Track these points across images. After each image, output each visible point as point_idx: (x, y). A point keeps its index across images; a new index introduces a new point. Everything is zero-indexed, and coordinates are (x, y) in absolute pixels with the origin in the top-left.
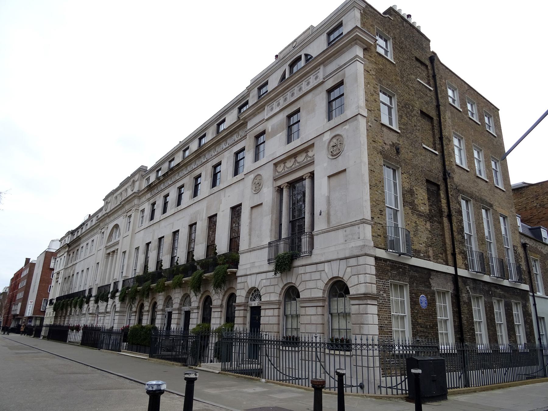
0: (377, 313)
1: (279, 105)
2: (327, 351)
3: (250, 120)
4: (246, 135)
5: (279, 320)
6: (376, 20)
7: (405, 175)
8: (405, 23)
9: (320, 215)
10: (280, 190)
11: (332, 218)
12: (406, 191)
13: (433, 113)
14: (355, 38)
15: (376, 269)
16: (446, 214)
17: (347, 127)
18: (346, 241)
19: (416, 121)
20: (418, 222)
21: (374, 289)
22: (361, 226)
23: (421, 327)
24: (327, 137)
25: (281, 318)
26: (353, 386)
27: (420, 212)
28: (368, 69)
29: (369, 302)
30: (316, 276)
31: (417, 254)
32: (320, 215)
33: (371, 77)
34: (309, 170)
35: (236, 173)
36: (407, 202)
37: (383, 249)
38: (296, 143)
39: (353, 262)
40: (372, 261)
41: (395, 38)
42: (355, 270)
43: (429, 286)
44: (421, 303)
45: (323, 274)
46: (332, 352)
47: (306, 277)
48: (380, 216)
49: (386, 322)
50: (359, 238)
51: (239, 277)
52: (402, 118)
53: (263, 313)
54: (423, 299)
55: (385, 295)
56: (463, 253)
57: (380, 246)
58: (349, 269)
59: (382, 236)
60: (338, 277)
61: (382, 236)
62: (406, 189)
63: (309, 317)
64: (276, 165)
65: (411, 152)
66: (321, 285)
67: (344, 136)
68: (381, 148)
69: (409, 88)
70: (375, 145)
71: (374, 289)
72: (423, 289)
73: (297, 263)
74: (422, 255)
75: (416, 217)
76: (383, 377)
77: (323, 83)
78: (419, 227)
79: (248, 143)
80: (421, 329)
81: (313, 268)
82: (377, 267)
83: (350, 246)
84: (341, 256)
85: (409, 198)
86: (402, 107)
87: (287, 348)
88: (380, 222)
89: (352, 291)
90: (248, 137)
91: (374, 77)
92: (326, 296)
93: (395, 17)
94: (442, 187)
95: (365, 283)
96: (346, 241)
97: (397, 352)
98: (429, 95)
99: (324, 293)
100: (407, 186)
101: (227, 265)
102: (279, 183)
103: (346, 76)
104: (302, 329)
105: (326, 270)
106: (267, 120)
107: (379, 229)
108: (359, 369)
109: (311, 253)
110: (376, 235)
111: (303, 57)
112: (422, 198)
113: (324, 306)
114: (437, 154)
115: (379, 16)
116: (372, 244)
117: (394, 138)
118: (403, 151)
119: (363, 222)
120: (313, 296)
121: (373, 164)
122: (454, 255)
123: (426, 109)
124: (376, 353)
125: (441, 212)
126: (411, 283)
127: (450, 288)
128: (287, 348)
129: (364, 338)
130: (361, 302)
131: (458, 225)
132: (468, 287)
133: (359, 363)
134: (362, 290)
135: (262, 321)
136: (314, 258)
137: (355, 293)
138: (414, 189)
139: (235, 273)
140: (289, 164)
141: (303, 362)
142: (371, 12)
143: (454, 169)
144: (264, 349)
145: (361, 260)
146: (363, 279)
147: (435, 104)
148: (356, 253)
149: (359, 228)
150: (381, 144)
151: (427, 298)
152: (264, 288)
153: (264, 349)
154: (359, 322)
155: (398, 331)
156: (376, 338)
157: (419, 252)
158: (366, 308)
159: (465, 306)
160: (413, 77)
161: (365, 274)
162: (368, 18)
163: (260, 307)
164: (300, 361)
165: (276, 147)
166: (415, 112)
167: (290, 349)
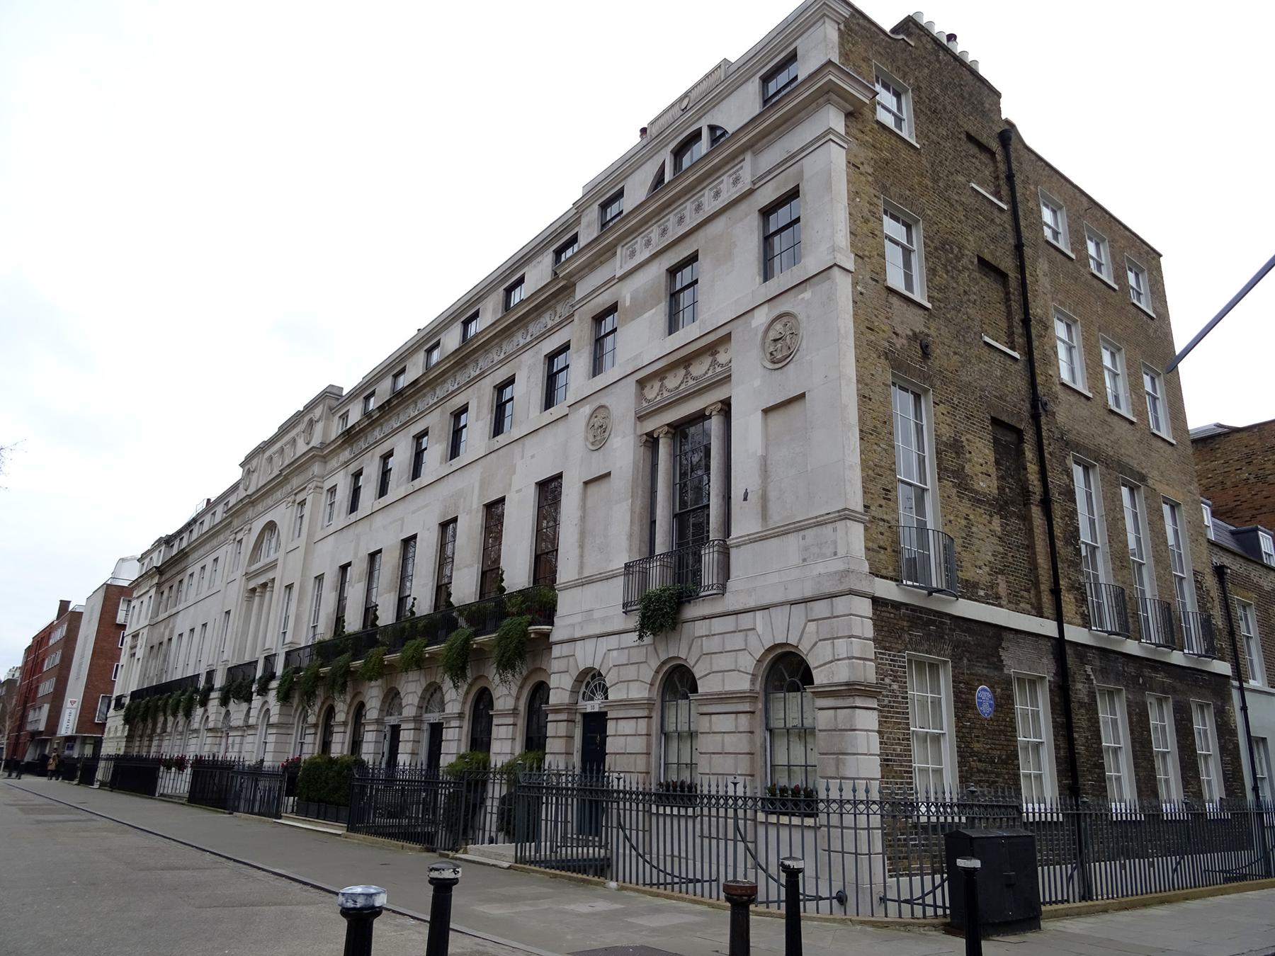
0: (876, 728)
1: (648, 243)
2: (761, 816)
3: (581, 278)
4: (572, 315)
5: (649, 745)
6: (875, 48)
7: (942, 408)
8: (941, 54)
9: (745, 499)
10: (651, 442)
11: (773, 508)
12: (946, 444)
13: (1007, 264)
14: (826, 89)
15: (875, 625)
16: (1038, 497)
17: (807, 295)
18: (804, 560)
19: (967, 280)
20: (971, 517)
21: (869, 673)
22: (840, 525)
23: (980, 761)
24: (761, 318)
25: (654, 739)
26: (821, 899)
27: (977, 492)
28: (857, 162)
29: (859, 702)
30: (736, 641)
31: (969, 590)
32: (745, 499)
33: (863, 178)
34: (718, 395)
35: (549, 402)
36: (946, 469)
37: (891, 579)
38: (688, 333)
39: (820, 608)
40: (865, 607)
41: (919, 88)
42: (825, 629)
43: (999, 666)
44: (980, 704)
45: (752, 638)
46: (773, 819)
47: (713, 644)
48: (883, 502)
49: (898, 748)
50: (835, 554)
51: (556, 643)
52: (934, 275)
53: (611, 727)
54: (983, 695)
55: (895, 686)
56: (1078, 589)
57: (884, 572)
58: (812, 627)
59: (889, 550)
60: (787, 644)
61: (889, 550)
62: (944, 439)
63: (718, 737)
64: (641, 383)
65: (955, 353)
66: (748, 663)
67: (799, 317)
68: (887, 344)
69: (952, 205)
70: (873, 338)
71: (869, 673)
72: (985, 671)
73: (692, 611)
74: (982, 593)
75: (968, 504)
76: (891, 876)
77: (751, 192)
78: (974, 529)
79: (578, 333)
80: (980, 765)
81: (729, 623)
82: (878, 621)
83: (815, 573)
84: (793, 596)
85: (951, 461)
86: (936, 249)
87: (668, 811)
88: (885, 517)
89: (819, 678)
90: (576, 318)
91: (870, 179)
92: (758, 687)
93: (919, 39)
94: (1029, 436)
95: (849, 658)
96: (804, 560)
97: (923, 819)
98: (997, 220)
99: (753, 682)
100: (947, 433)
101: (528, 617)
102: (650, 425)
103: (806, 176)
104: (703, 765)
105: (759, 629)
106: (622, 278)
107: (882, 534)
108: (836, 858)
109: (723, 589)
110: (875, 547)
111: (705, 134)
112: (981, 461)
113: (753, 713)
114: (1016, 359)
115: (882, 36)
116: (866, 567)
117: (916, 322)
118: (937, 351)
119: (845, 515)
120: (728, 688)
121: (869, 381)
122: (1056, 592)
123: (992, 253)
124: (876, 821)
125: (1025, 493)
126: (956, 659)
127: (1046, 669)
128: (668, 811)
129: (848, 785)
130: (840, 703)
131: (1067, 524)
132: (1088, 668)
133: (836, 845)
134: (842, 674)
135: (610, 747)
136: (732, 601)
137: (825, 682)
138: (963, 439)
139: (547, 635)
140: (672, 381)
141: (706, 841)
142: (863, 28)
143: (1056, 393)
144: (615, 811)
145: (841, 605)
146: (844, 650)
147: (1012, 241)
148: (828, 588)
149: (835, 530)
150: (886, 336)
151: (994, 692)
152: (614, 670)
153: (615, 811)
154: (836, 750)
155: (927, 770)
156: (875, 786)
157: (975, 585)
158: (852, 718)
159: (1083, 711)
160: (961, 179)
161: (850, 637)
162: (857, 43)
163: (606, 713)
164: (698, 841)
165: (642, 341)
166: (965, 261)
167: (675, 811)
